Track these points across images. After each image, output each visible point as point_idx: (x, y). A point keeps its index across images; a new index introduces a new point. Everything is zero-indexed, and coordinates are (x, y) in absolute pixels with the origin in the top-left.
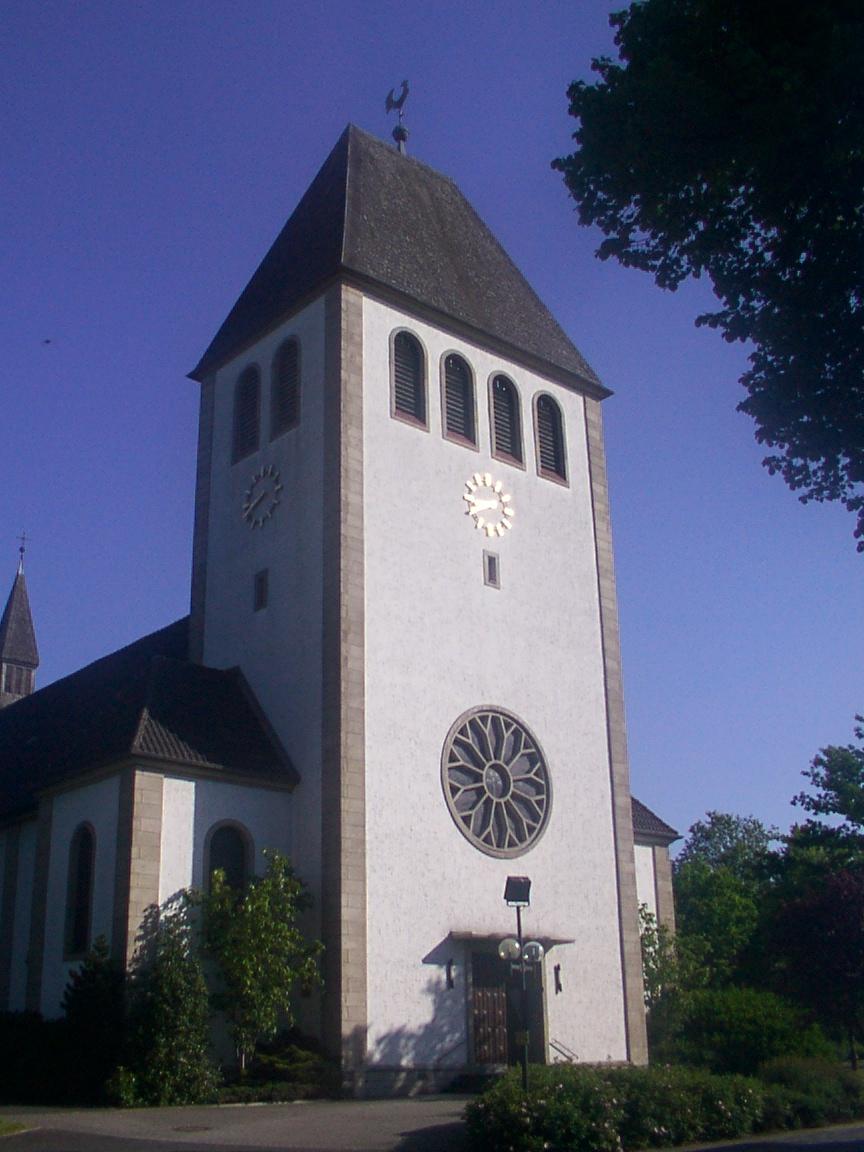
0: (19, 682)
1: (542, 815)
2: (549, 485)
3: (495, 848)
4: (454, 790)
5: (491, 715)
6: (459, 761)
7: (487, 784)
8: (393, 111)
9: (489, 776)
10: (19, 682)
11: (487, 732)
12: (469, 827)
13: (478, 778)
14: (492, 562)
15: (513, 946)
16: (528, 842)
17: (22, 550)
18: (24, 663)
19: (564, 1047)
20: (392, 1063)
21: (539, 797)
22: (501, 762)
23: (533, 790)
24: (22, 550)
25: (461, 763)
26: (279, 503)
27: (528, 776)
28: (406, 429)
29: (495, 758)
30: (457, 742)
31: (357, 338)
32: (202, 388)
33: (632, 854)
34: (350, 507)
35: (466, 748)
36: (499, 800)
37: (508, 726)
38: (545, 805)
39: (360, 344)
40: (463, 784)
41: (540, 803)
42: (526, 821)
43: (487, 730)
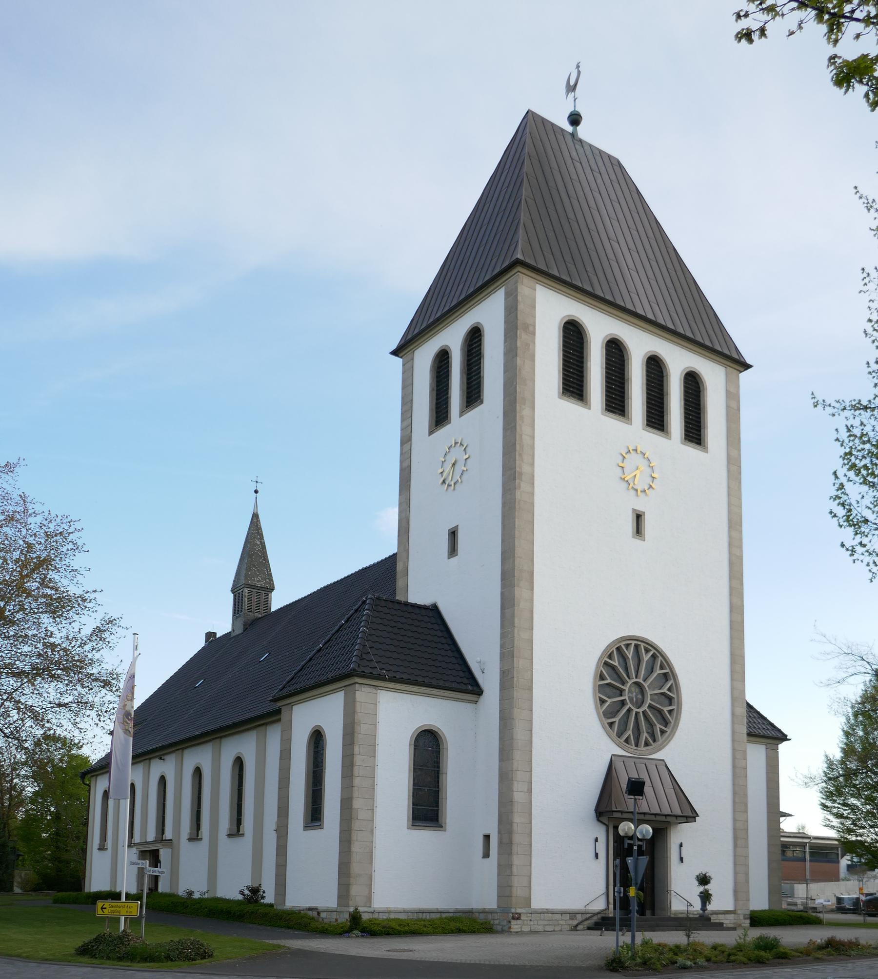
0: (258, 604)
1: (673, 722)
2: (691, 451)
3: (634, 747)
4: (602, 702)
5: (634, 643)
6: (607, 679)
7: (629, 697)
8: (571, 95)
9: (629, 692)
10: (258, 604)
11: (630, 656)
12: (614, 732)
13: (621, 692)
14: (639, 530)
15: (630, 828)
16: (660, 743)
17: (256, 492)
18: (262, 588)
19: (347, 804)
20: (801, 6)
21: (670, 708)
22: (641, 681)
23: (667, 701)
24: (256, 492)
25: (609, 681)
26: (467, 470)
27: (661, 691)
28: (571, 407)
29: (636, 678)
30: (606, 663)
31: (531, 328)
32: (404, 365)
33: (745, 752)
34: (523, 476)
35: (613, 668)
36: (638, 710)
37: (647, 651)
38: (676, 713)
39: (534, 334)
40: (609, 698)
41: (670, 712)
42: (658, 726)
43: (630, 654)
